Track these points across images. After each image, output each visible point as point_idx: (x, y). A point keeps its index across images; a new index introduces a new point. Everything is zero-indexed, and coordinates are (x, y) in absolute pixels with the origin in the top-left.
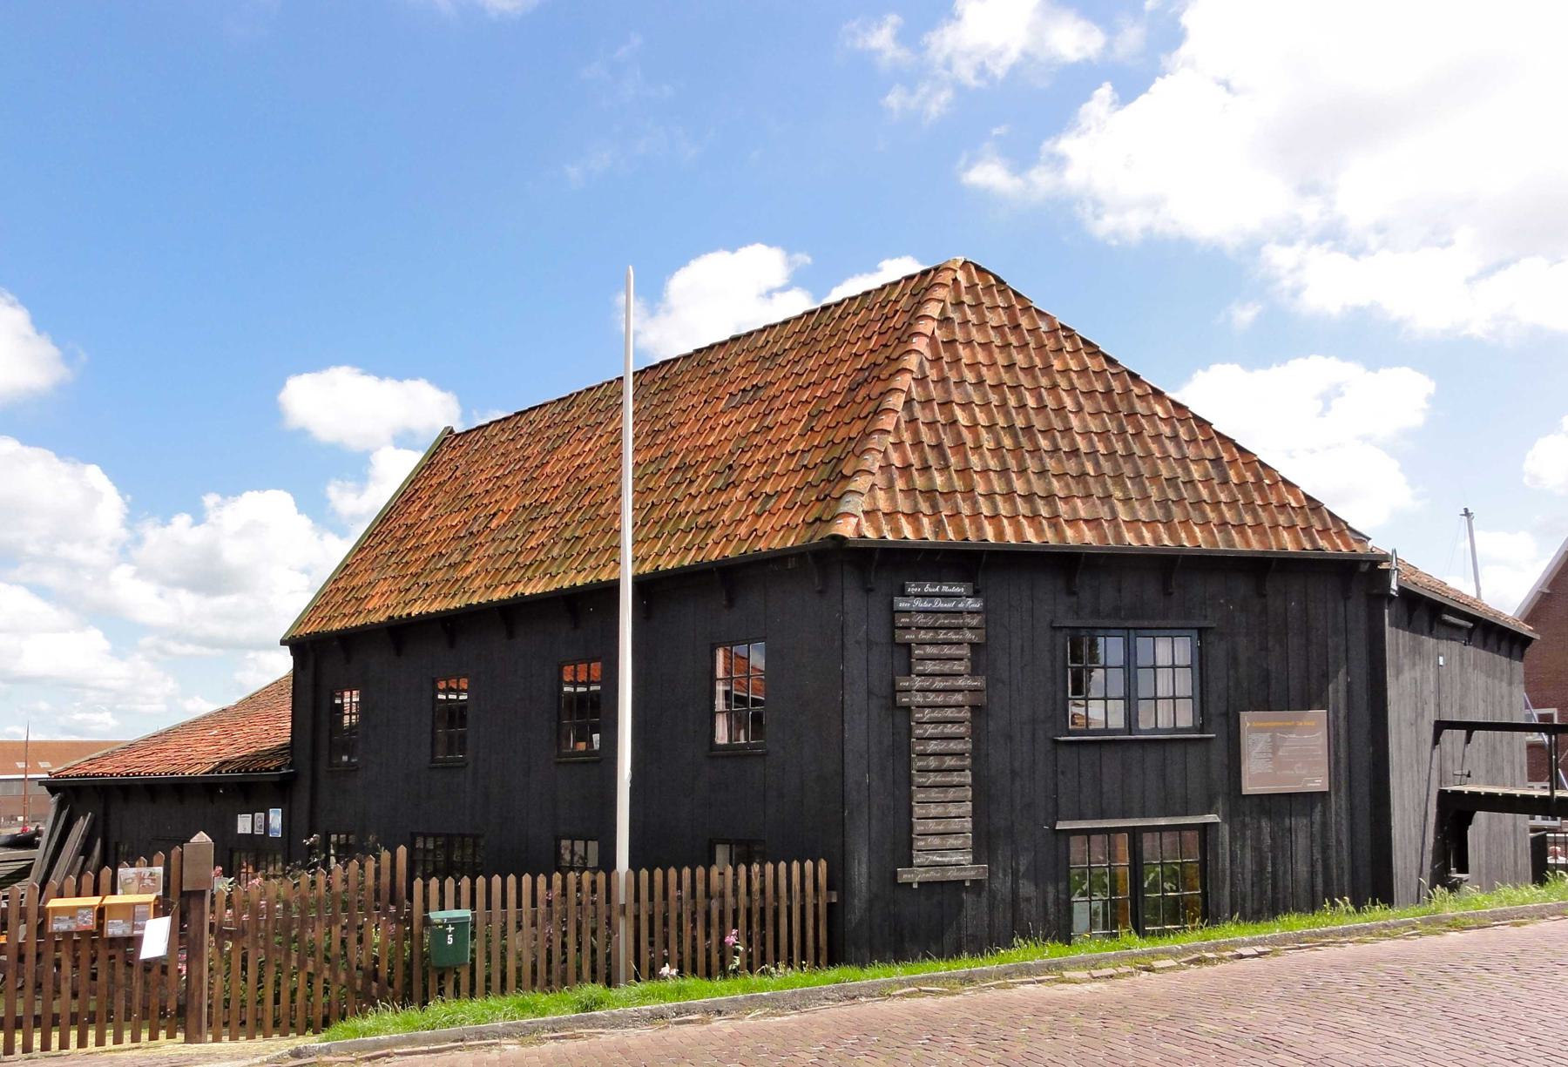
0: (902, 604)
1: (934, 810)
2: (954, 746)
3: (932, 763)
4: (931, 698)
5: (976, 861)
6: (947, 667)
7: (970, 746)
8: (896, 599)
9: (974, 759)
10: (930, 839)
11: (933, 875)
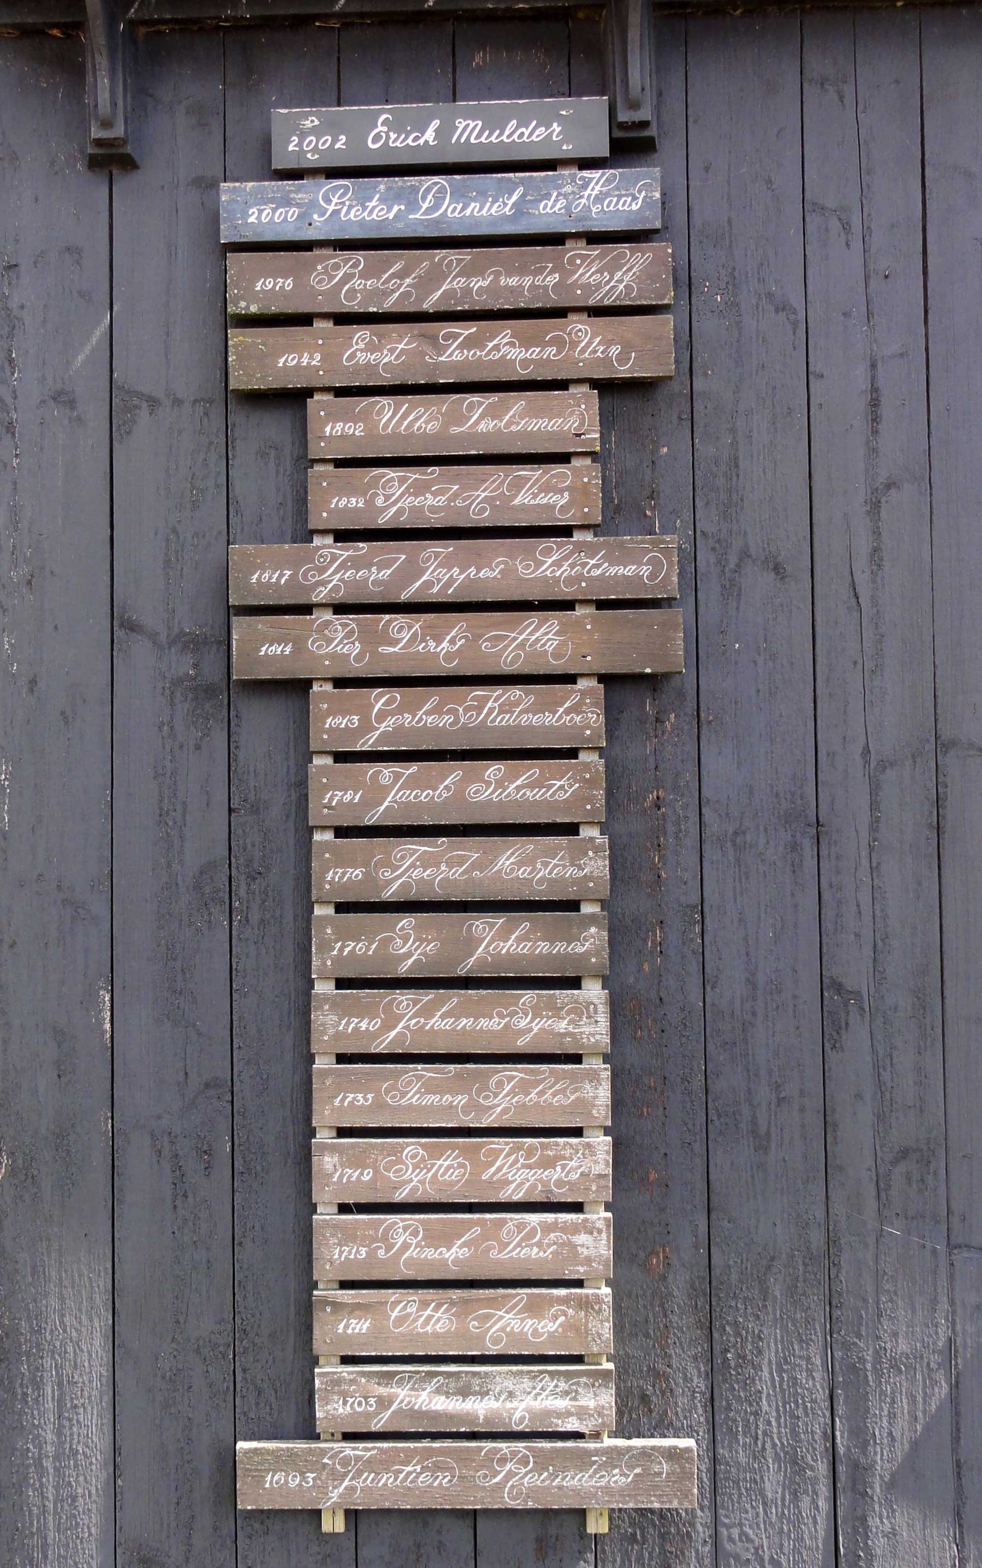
0: (260, 211)
1: (417, 1170)
2: (514, 866)
3: (410, 944)
4: (404, 642)
5: (636, 1413)
6: (481, 496)
7: (597, 866)
8: (228, 191)
9: (620, 934)
10: (402, 1305)
11: (412, 1480)
